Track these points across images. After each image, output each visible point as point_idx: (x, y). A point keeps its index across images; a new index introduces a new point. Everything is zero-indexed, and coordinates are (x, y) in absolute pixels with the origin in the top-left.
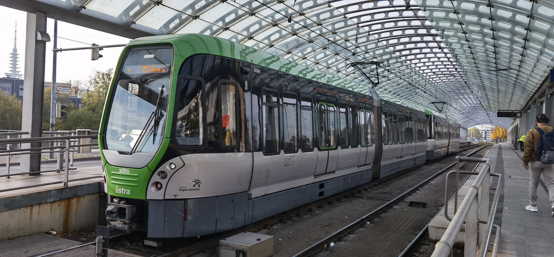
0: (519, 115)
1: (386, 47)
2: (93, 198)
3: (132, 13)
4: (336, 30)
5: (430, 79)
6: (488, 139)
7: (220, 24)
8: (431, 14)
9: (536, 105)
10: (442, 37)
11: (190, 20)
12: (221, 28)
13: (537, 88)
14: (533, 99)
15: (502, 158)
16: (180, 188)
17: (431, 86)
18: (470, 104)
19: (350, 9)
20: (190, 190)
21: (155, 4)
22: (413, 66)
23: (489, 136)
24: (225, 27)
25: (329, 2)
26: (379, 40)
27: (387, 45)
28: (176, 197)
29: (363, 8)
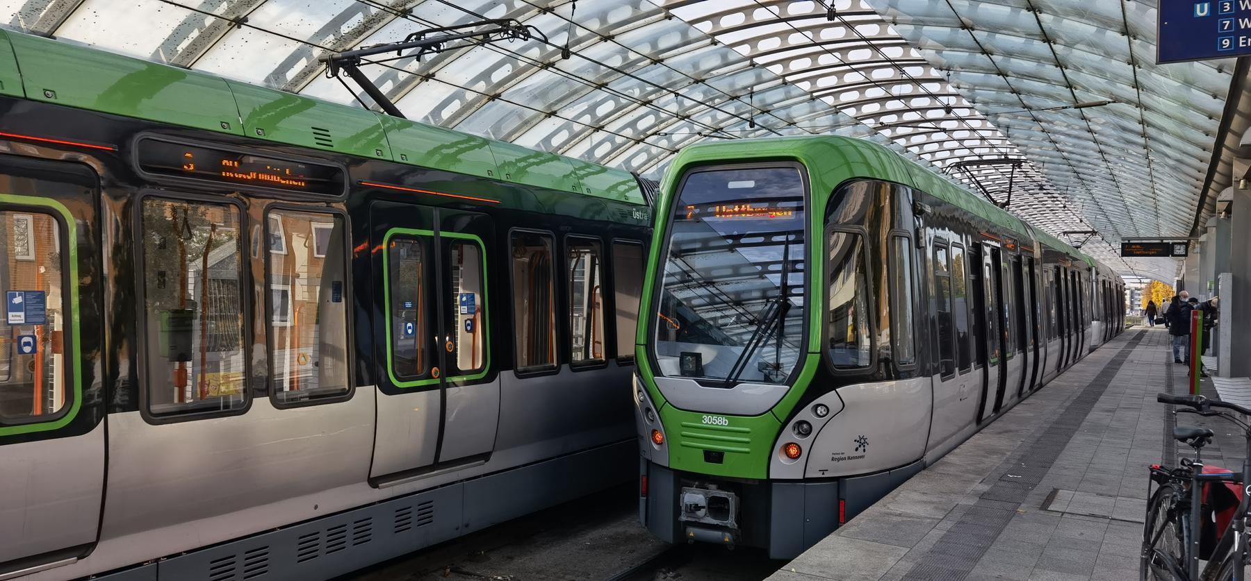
0: (1180, 250)
1: (812, 96)
2: (1141, 297)
6: (1139, 308)
10: (955, 85)
12: (414, 75)
16: (833, 456)
19: (726, 22)
20: (849, 458)
21: (229, 25)
23: (1140, 303)
24: (493, 94)
25: (668, 8)
28: (823, 474)
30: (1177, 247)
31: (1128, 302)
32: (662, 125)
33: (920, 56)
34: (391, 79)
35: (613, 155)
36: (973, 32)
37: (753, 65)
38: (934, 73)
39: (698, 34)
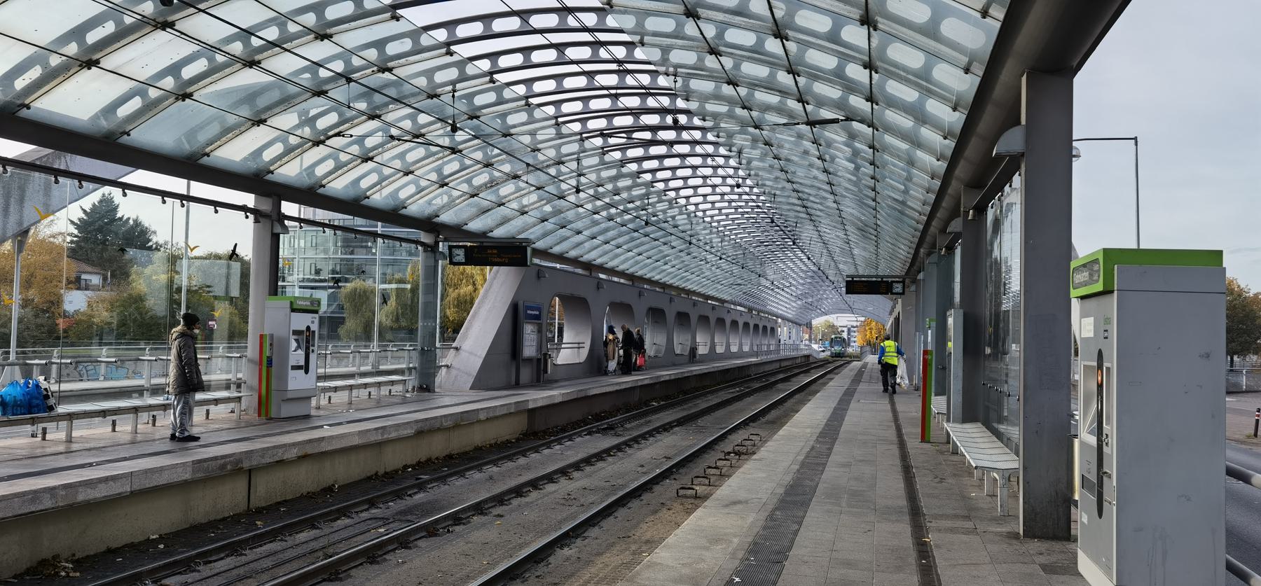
0: (898, 288)
1: (581, 137)
2: (856, 334)
3: (20, 84)
4: (563, 157)
5: (705, 219)
7: (169, 83)
8: (686, 85)
9: (934, 258)
10: (701, 117)
11: (243, 129)
13: (925, 218)
14: (928, 239)
15: (884, 386)
17: (711, 233)
18: (802, 271)
19: (463, 31)
22: (692, 208)
23: (855, 339)
25: (394, 7)
26: (604, 151)
27: (606, 147)
29: (532, 62)
30: (895, 285)
31: (1001, 318)
32: (346, 126)
33: (668, 85)
34: (333, 159)
35: (286, 159)
36: (737, 88)
37: (528, 104)
38: (697, 122)
39: (477, 72)
